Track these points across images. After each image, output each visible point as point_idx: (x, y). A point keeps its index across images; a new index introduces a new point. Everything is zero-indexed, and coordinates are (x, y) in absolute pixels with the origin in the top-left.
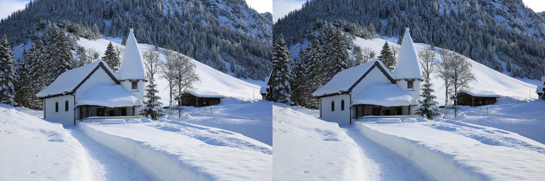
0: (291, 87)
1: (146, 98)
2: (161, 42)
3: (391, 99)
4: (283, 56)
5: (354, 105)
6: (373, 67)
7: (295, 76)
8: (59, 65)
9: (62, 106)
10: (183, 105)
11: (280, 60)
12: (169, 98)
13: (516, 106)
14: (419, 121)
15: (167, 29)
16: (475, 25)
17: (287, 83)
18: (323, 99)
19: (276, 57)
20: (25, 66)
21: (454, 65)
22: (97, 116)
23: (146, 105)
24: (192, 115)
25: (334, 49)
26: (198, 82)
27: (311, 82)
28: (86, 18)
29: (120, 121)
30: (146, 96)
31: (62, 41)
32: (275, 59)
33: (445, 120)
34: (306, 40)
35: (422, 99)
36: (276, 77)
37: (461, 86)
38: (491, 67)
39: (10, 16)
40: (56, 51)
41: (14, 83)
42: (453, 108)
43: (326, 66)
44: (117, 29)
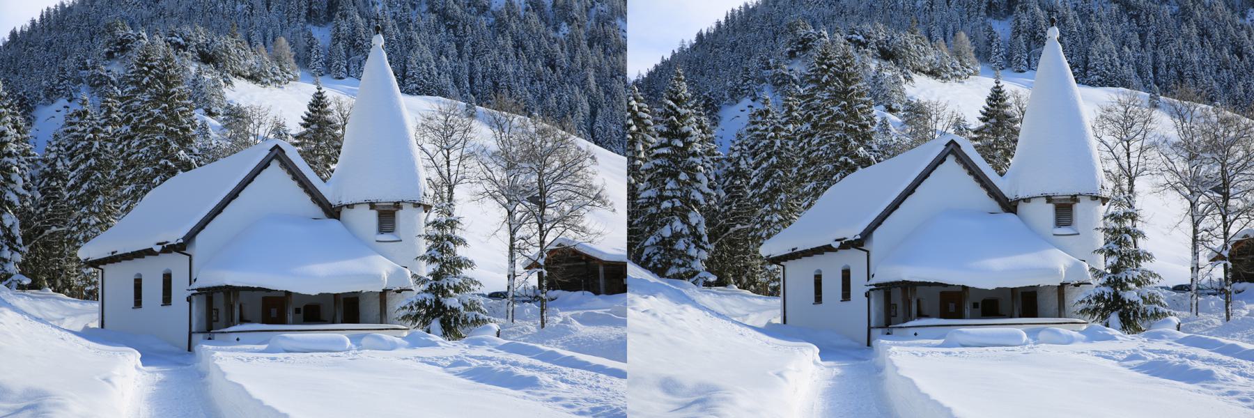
0: (707, 231)
2: (482, 90)
5: (878, 286)
7: (723, 194)
9: (152, 290)
10: (552, 285)
11: (676, 147)
14: (414, 343)
15: (1188, 37)
16: (607, 36)
17: (695, 217)
19: (665, 140)
21: (536, 157)
22: (265, 321)
23: (1104, 280)
24: (584, 321)
25: (156, 111)
26: (600, 211)
29: (1010, 336)
30: (423, 258)
31: (845, 81)
32: (662, 146)
33: (501, 341)
35: (425, 270)
36: (662, 198)
37: (559, 228)
39: (723, 20)
41: (710, 216)
42: (535, 298)
43: (133, 166)
44: (347, 52)
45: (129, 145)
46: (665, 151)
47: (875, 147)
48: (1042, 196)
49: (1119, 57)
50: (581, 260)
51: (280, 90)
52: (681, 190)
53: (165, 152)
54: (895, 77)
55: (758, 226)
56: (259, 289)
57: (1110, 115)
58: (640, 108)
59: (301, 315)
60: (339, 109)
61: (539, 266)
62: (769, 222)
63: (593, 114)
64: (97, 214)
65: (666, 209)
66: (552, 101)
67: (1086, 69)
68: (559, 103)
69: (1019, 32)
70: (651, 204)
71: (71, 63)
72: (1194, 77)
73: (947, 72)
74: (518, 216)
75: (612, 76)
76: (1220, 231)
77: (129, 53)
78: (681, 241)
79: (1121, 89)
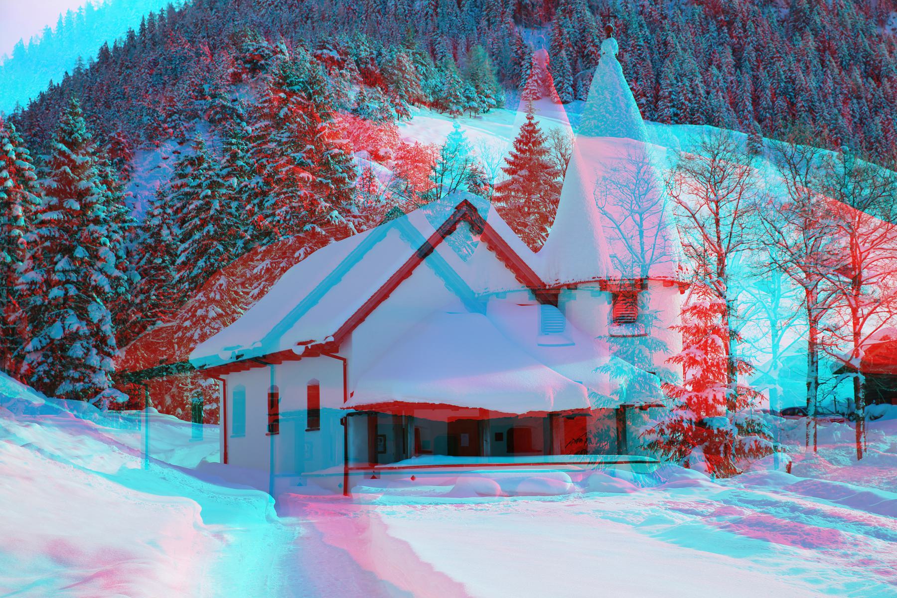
1: (679, 368)
6: (447, 230)
11: (70, 211)
17: (98, 311)
18: (234, 380)
19: (54, 201)
20: (165, 232)
23: (683, 400)
25: (298, 155)
27: (201, 304)
28: (445, 26)
30: (678, 359)
31: (311, 116)
32: (51, 208)
33: (793, 479)
39: (137, 29)
42: (850, 416)
45: (260, 205)
46: (54, 215)
47: (355, 211)
48: (595, 280)
51: (476, 122)
52: (77, 271)
53: (312, 212)
55: (187, 323)
56: (442, 406)
58: (19, 155)
59: (503, 444)
60: (559, 146)
61: (853, 370)
62: (204, 318)
64: (218, 303)
65: (55, 299)
67: (657, 98)
68: (885, 131)
69: (561, 46)
70: (33, 292)
71: (183, 90)
73: (458, 103)
74: (821, 296)
76: (848, 330)
77: (262, 75)
78: (78, 344)
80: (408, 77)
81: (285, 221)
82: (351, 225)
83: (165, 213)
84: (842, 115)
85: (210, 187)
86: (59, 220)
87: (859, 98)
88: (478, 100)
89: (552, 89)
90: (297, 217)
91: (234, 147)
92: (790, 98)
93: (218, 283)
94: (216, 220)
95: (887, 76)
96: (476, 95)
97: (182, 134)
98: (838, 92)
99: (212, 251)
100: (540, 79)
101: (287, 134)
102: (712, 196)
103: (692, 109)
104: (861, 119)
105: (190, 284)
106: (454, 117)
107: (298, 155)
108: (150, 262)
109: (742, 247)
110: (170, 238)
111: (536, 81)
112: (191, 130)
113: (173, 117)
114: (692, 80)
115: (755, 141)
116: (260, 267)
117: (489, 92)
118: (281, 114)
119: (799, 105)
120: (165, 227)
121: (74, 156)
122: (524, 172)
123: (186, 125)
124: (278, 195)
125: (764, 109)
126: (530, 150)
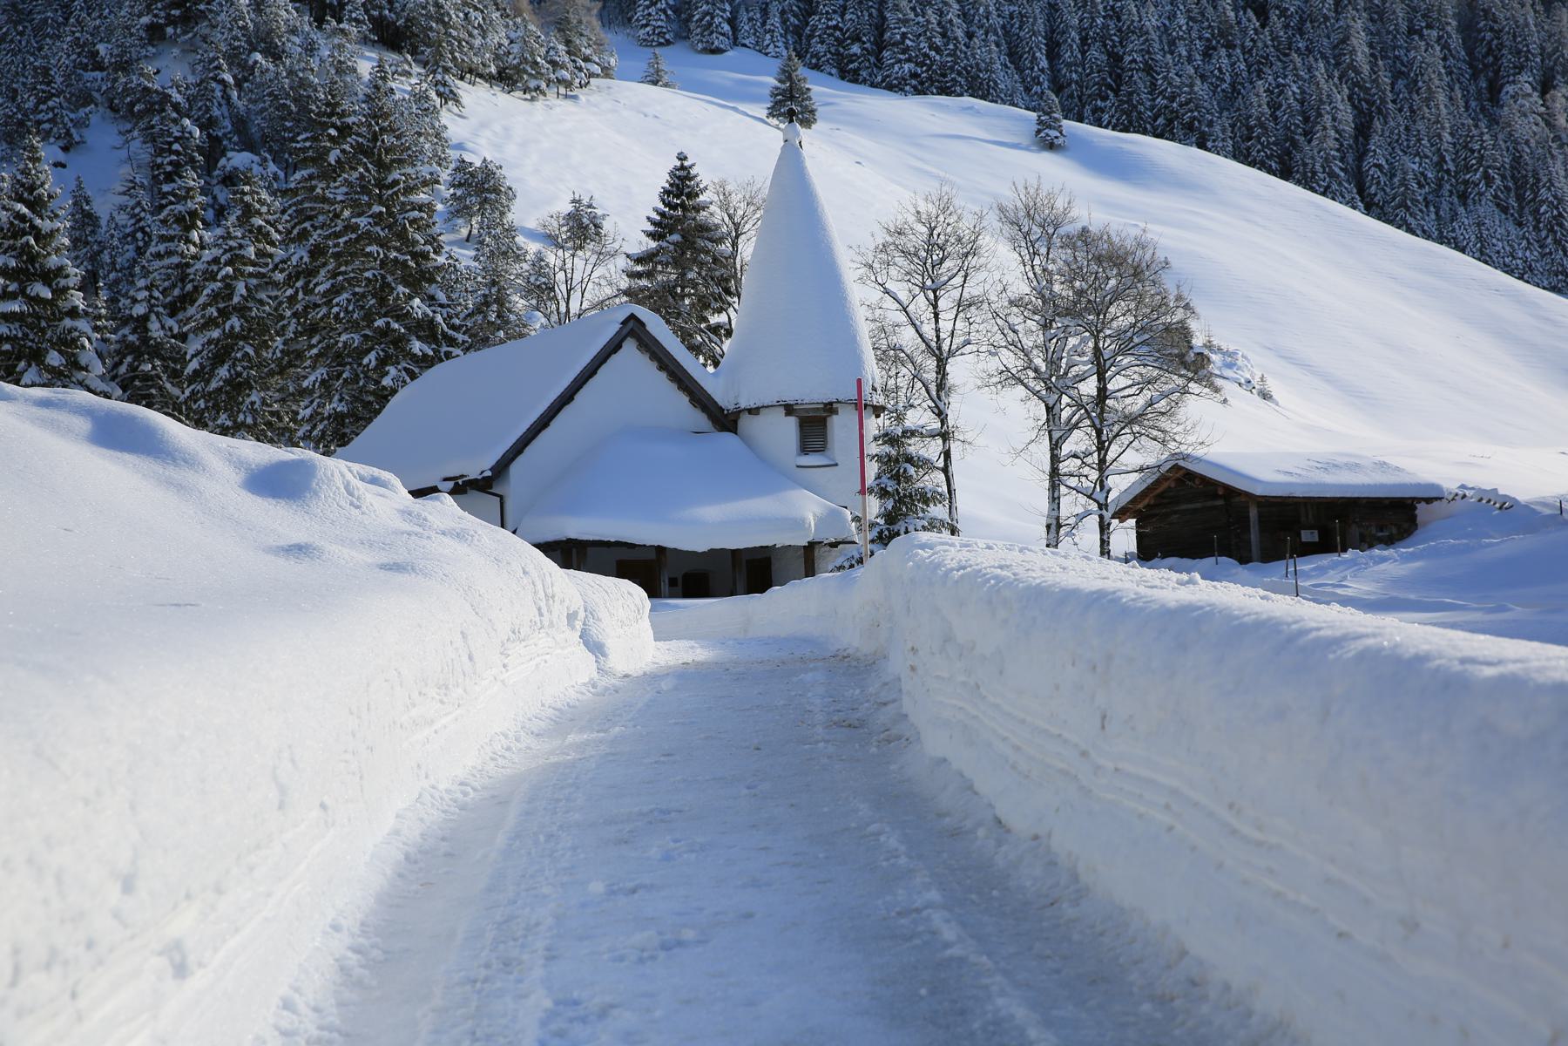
3: (712, 513)
4: (50, 277)
6: (613, 347)
8: (369, 318)
12: (1044, 504)
13: (1500, 546)
20: (154, 326)
25: (363, 222)
34: (97, 116)
38: (1524, 273)
40: (350, 228)
45: (307, 291)
48: (778, 405)
49: (964, 15)
50: (1215, 496)
53: (382, 301)
54: (421, 97)
56: (618, 544)
57: (901, 240)
59: (679, 588)
63: (1363, 130)
66: (1258, 100)
67: (880, 45)
68: (1274, 106)
71: (60, 55)
72: (1149, 69)
74: (1065, 415)
75: (1412, 31)
77: (203, 28)
79: (967, 100)
80: (454, 33)
81: (347, 311)
82: (439, 319)
83: (151, 296)
84: (1203, 77)
85: (229, 263)
86: (22, 313)
87: (1230, 46)
88: (570, 65)
89: (692, 26)
90: (362, 307)
91: (247, 198)
92: (1114, 46)
93: (248, 401)
94: (241, 310)
95: (1278, 7)
96: (567, 59)
97: (68, 133)
98: (1194, 35)
99: (239, 355)
100: (671, 7)
101: (344, 189)
102: (929, 283)
103: (943, 65)
104: (1233, 85)
105: (207, 401)
106: (533, 99)
107: (363, 222)
108: (133, 368)
109: (968, 348)
110: (162, 333)
111: (664, 11)
112: (81, 124)
113: (50, 103)
114: (941, 13)
115: (1050, 127)
116: (312, 378)
117: (588, 52)
118: (332, 159)
119: (1128, 58)
120: (153, 317)
121: (38, 221)
122: (676, 237)
123: (72, 116)
124: (334, 275)
125: (1069, 65)
126: (683, 205)
